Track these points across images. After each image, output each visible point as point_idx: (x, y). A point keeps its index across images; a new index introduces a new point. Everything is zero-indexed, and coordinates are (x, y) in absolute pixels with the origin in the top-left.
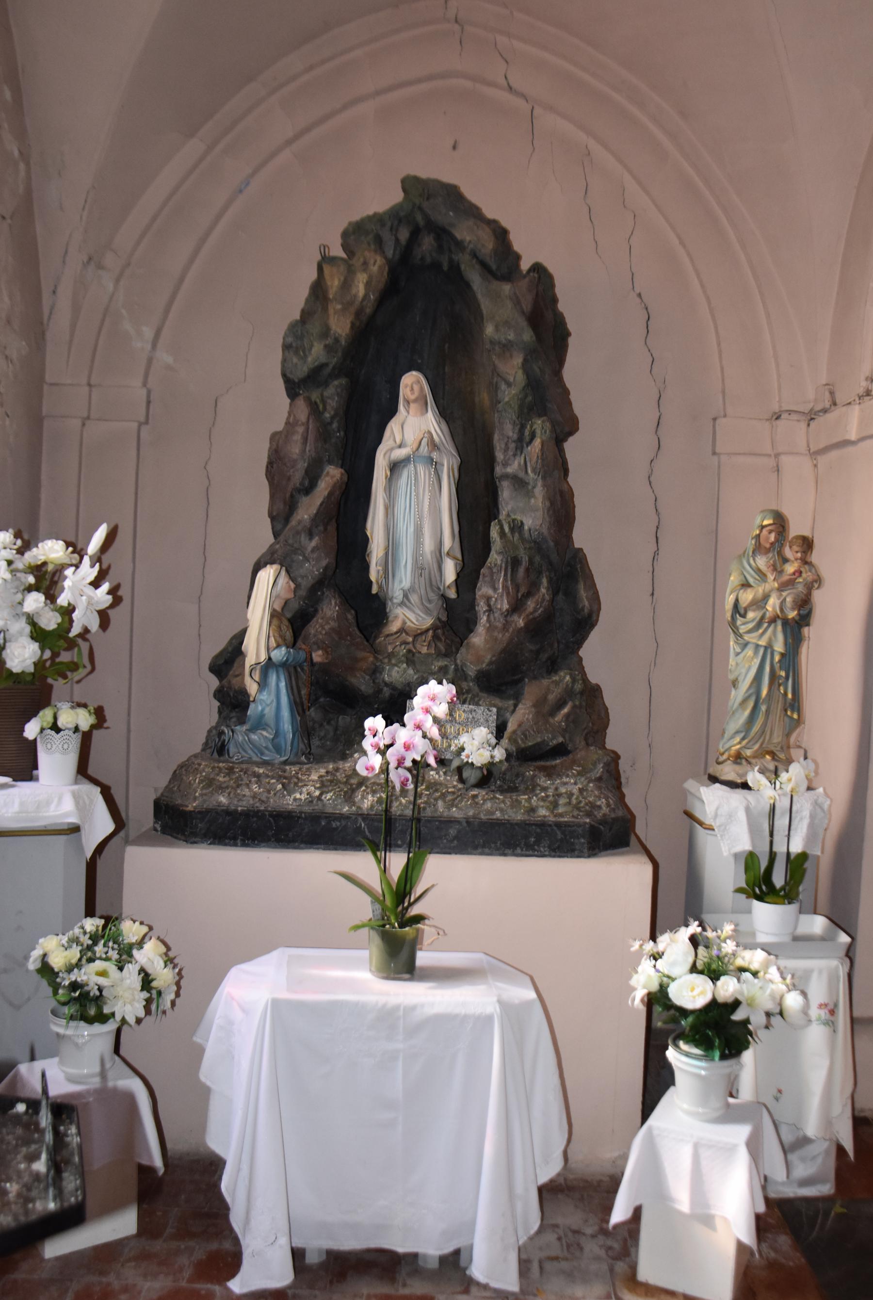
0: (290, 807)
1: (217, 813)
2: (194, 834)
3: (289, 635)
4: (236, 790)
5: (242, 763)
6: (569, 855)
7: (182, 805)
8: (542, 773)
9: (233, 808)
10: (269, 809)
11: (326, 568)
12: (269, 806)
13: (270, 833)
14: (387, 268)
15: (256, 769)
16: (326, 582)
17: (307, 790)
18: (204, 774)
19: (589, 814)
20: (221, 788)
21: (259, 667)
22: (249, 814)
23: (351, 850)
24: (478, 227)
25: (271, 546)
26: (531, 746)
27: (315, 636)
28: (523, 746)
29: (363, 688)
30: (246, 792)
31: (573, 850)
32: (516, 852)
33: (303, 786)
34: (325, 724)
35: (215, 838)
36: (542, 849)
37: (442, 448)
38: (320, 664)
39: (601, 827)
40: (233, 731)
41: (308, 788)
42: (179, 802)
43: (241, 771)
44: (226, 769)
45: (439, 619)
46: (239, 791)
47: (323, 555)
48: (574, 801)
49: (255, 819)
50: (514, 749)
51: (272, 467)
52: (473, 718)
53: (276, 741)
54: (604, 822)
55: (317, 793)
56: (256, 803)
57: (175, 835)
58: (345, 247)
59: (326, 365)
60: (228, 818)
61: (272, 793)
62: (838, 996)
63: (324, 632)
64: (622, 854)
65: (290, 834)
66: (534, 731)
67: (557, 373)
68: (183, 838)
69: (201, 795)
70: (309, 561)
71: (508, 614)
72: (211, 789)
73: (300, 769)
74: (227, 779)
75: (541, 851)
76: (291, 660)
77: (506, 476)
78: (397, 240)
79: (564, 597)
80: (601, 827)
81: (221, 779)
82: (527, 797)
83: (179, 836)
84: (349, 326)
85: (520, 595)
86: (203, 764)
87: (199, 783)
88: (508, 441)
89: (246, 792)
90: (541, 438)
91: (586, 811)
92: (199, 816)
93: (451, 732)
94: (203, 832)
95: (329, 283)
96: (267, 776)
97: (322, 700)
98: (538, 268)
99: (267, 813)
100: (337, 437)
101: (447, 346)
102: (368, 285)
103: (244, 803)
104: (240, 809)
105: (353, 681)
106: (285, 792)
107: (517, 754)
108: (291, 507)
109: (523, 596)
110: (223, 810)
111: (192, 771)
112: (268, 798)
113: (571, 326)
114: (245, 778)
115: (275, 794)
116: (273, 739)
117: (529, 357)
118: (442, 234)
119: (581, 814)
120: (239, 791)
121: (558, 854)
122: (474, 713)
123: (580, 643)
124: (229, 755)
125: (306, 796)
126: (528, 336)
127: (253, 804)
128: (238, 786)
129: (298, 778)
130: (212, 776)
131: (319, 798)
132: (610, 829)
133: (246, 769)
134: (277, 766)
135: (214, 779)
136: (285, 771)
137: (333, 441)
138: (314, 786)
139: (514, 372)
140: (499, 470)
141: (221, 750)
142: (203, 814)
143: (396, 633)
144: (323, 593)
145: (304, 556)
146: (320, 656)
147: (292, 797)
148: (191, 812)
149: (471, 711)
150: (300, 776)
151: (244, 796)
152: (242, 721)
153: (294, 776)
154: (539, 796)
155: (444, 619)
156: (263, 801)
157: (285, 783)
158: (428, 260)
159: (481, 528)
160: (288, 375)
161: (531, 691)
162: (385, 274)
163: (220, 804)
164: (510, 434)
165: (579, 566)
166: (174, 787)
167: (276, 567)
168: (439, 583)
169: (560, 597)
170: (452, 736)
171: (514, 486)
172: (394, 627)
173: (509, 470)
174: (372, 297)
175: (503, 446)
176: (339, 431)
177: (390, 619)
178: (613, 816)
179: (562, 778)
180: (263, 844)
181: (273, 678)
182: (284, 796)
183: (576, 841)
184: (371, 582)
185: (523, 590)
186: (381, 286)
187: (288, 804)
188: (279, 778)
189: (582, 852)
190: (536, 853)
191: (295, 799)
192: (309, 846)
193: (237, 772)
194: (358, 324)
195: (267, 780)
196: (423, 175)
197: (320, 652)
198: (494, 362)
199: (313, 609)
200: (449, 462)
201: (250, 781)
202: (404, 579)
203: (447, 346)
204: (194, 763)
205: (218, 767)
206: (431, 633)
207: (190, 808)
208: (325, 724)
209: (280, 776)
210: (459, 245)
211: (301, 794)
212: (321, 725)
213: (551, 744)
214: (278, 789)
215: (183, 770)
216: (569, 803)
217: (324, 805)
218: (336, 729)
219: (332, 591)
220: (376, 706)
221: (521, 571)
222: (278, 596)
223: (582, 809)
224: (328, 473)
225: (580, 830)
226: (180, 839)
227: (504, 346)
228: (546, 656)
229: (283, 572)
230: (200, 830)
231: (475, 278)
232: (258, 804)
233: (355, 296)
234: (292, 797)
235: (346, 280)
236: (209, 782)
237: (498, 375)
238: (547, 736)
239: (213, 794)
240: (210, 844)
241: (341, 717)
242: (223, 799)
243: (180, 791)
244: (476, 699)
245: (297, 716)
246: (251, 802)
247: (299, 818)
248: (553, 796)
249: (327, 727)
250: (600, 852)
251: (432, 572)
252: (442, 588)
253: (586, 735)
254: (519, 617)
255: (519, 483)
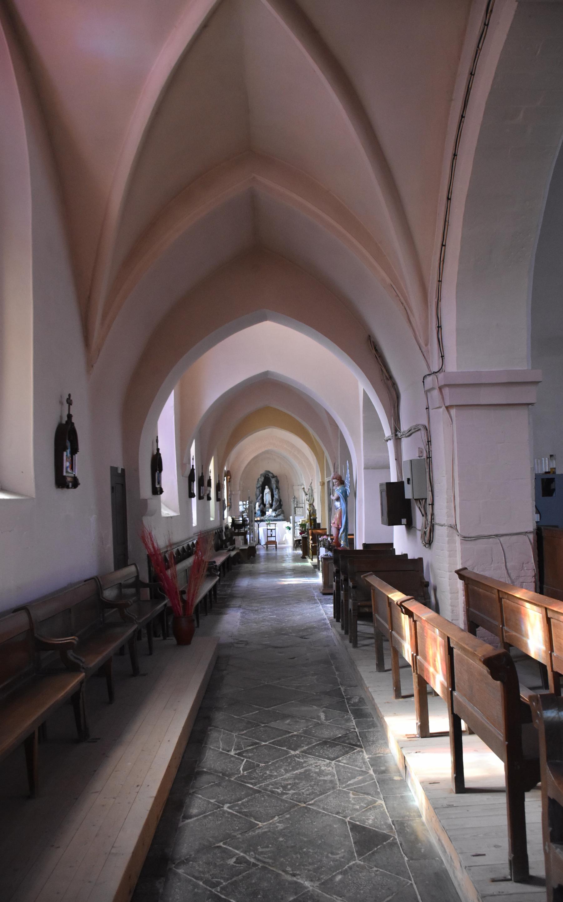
23: (337, 348)
62: (381, 618)
90: (201, 885)
108: (258, 498)
118: (268, 475)
161: (278, 511)
200: (270, 493)
231: (271, 478)
255: (276, 494)
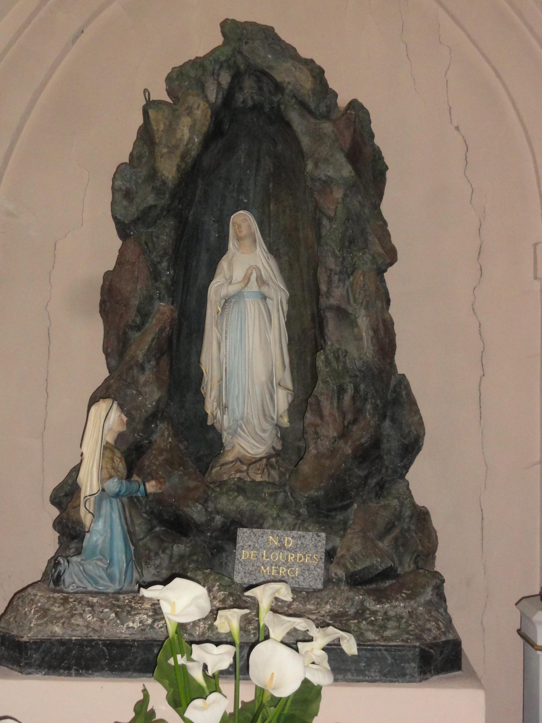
0: (124, 636)
1: (51, 643)
2: (29, 665)
3: (121, 466)
4: (70, 620)
5: (76, 593)
6: (400, 680)
7: (17, 636)
8: (372, 597)
9: (67, 638)
10: (103, 638)
11: (158, 401)
12: (102, 635)
13: (103, 662)
14: (209, 112)
15: (90, 598)
16: (160, 415)
17: (140, 618)
18: (39, 604)
19: (418, 638)
20: (55, 619)
21: (92, 498)
22: (82, 644)
24: (296, 68)
25: (106, 380)
26: (360, 571)
27: (149, 466)
28: (352, 570)
29: (195, 516)
30: (80, 621)
31: (404, 675)
32: (346, 677)
33: (135, 615)
34: (160, 552)
35: (49, 669)
36: (372, 674)
37: (271, 283)
38: (155, 494)
39: (432, 651)
40: (68, 562)
41: (140, 616)
42: (15, 633)
43: (74, 601)
44: (61, 599)
45: (273, 448)
46: (73, 621)
47: (155, 389)
48: (403, 626)
49: (89, 649)
50: (344, 574)
51: (105, 306)
52: (302, 543)
53: (109, 570)
54: (433, 645)
55: (150, 621)
56: (90, 632)
57: (10, 666)
58: (170, 92)
59: (155, 206)
60: (62, 648)
61: (106, 622)
63: (157, 463)
64: (455, 677)
65: (124, 663)
66: (363, 555)
67: (376, 206)
68: (18, 668)
69: (35, 625)
70: (142, 395)
71: (335, 441)
72: (45, 620)
73: (133, 598)
74: (61, 609)
75: (372, 676)
76: (123, 491)
77: (331, 308)
78: (219, 84)
79: (390, 423)
80: (432, 651)
81: (56, 609)
82: (356, 621)
83: (15, 667)
84: (175, 169)
85: (346, 423)
86: (39, 594)
87: (34, 614)
88: (331, 274)
89: (80, 621)
91: (415, 635)
92: (34, 647)
93: (279, 559)
94: (38, 662)
95: (155, 128)
96: (101, 606)
97: (157, 529)
98: (354, 105)
99: (100, 643)
100: (168, 275)
101: (271, 185)
102: (192, 128)
103: (78, 633)
104: (74, 638)
105: (187, 510)
106: (118, 621)
107: (346, 578)
109: (349, 423)
110: (57, 640)
111: (27, 602)
112: (101, 627)
113: (388, 159)
114: (78, 607)
115: (108, 623)
116: (107, 569)
117: (348, 192)
119: (411, 637)
120: (73, 621)
121: (388, 679)
122: (302, 539)
123: (407, 468)
124: (64, 585)
125: (139, 625)
126: (347, 171)
127: (87, 634)
128: (73, 616)
129: (131, 607)
130: (47, 606)
131: (152, 626)
132: (442, 653)
133: (80, 598)
134: (111, 595)
135: (48, 609)
136: (118, 600)
137: (164, 279)
138: (146, 614)
139: (334, 207)
140: (323, 302)
141: (58, 580)
142: (38, 644)
143: (232, 462)
144: (157, 426)
145: (138, 391)
146: (153, 487)
147: (125, 626)
148: (26, 642)
149: (300, 538)
150: (133, 605)
151: (78, 625)
152: (79, 552)
153: (127, 605)
154: (369, 620)
155: (279, 447)
156: (96, 631)
157: (118, 612)
158: (250, 103)
159: (309, 359)
160: (119, 217)
162: (209, 117)
163: (54, 634)
164: (333, 266)
165: (404, 393)
166: (10, 618)
167: (109, 401)
168: (272, 413)
169: (387, 423)
170: (280, 563)
171: (338, 316)
172: (230, 457)
173: (333, 301)
174: (196, 140)
175: (326, 279)
176: (168, 270)
177: (227, 449)
178: (444, 639)
179: (391, 602)
180: (96, 674)
181: (106, 507)
182: (117, 625)
183: (407, 665)
184: (207, 414)
185: (350, 417)
186: (205, 129)
187: (122, 633)
188: (112, 607)
189: (413, 676)
190: (367, 678)
191: (128, 628)
192: (142, 674)
193: (72, 602)
194: (183, 166)
195: (101, 610)
196: (241, 18)
197: (153, 483)
198: (315, 198)
199: (147, 442)
201: (84, 611)
202: (237, 409)
203: (271, 185)
204: (30, 594)
205: (53, 597)
206: (265, 461)
207: (25, 639)
208: (160, 552)
209: (114, 605)
210: (278, 87)
211: (133, 623)
212: (157, 554)
213: (379, 567)
214: (111, 618)
215: (20, 600)
216: (399, 627)
217: (157, 633)
218: (171, 557)
219: (166, 423)
220: (209, 534)
221: (347, 398)
222: (110, 430)
223: (412, 633)
224: (159, 310)
225: (410, 654)
226: (16, 670)
227: (325, 182)
228: (375, 481)
229: (115, 406)
230: (35, 661)
232: (91, 634)
233: (181, 140)
234: (125, 626)
235: (170, 125)
236: (44, 612)
237: (320, 210)
238: (376, 560)
239: (47, 624)
240: (45, 674)
241: (175, 547)
242: (58, 629)
243: (16, 622)
244: (306, 525)
245: (131, 545)
246: (85, 631)
247: (131, 646)
248: (383, 620)
249: (162, 555)
250: (432, 676)
251: (265, 403)
252: (275, 418)
253: (416, 558)
254: (346, 443)
